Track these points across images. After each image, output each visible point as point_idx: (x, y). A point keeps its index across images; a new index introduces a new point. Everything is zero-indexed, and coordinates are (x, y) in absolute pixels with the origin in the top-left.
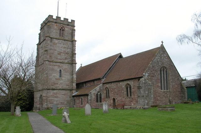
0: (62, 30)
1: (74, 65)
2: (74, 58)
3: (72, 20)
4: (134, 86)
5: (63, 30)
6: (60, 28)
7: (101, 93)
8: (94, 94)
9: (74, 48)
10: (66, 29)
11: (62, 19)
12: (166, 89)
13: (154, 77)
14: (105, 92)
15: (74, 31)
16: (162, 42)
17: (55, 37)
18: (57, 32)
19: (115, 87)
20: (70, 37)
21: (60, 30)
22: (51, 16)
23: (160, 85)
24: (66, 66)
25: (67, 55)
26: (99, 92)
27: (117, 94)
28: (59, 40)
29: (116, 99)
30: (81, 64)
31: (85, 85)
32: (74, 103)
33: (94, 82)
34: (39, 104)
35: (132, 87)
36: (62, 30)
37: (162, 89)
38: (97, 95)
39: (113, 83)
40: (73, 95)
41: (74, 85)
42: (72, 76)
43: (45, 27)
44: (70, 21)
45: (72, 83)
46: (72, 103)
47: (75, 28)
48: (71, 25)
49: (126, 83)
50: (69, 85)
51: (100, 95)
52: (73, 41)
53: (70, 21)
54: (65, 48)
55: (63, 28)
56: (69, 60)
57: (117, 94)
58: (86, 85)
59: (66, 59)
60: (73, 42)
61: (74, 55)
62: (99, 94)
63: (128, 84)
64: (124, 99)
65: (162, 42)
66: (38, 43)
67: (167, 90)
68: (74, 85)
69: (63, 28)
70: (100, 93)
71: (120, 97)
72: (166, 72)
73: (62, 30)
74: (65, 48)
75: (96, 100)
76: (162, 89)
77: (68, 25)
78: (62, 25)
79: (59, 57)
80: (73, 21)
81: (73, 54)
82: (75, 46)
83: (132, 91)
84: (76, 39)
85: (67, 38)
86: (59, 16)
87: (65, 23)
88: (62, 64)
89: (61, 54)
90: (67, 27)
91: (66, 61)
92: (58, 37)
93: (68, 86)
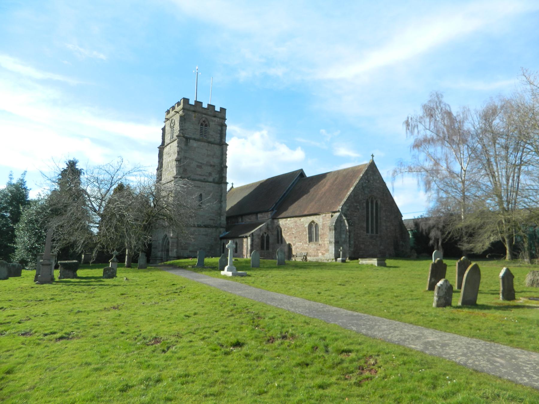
0: (204, 125)
1: (223, 185)
2: (223, 175)
3: (196, 102)
4: (323, 225)
5: (206, 126)
6: (201, 121)
7: (269, 235)
8: (258, 235)
9: (224, 156)
10: (211, 123)
11: (205, 106)
12: (375, 232)
13: (356, 212)
14: (275, 233)
15: (224, 128)
16: (373, 156)
17: (193, 137)
18: (195, 129)
19: (292, 225)
20: (217, 137)
21: (202, 125)
22: (201, 103)
23: (365, 225)
24: (209, 187)
25: (210, 169)
26: (265, 233)
27: (295, 237)
28: (199, 143)
29: (294, 245)
30: (232, 184)
31: (240, 220)
32: (222, 251)
33: (257, 215)
34: (162, 251)
35: (320, 227)
36: (204, 126)
37: (368, 232)
38: (263, 237)
39: (289, 219)
40: (221, 236)
41: (223, 219)
42: (220, 205)
43: (174, 118)
44: (217, 109)
45: (220, 216)
46: (218, 249)
47: (227, 122)
48: (220, 115)
49: (310, 219)
50: (214, 220)
51: (268, 237)
52: (223, 145)
53: (217, 109)
54: (208, 156)
55: (207, 123)
56: (215, 176)
57: (295, 237)
58: (242, 220)
59: (210, 174)
60: (223, 145)
61: (224, 169)
62: (265, 236)
63: (313, 222)
64: (307, 245)
65: (373, 156)
66: (161, 146)
67: (377, 233)
68: (222, 219)
69: (207, 123)
70: (268, 235)
71: (300, 242)
72: (377, 204)
73: (204, 125)
74: (208, 156)
75: (260, 246)
76: (368, 232)
77: (215, 116)
78: (204, 116)
79: (199, 171)
80: (223, 110)
81: (222, 169)
82: (226, 154)
83: (365, 211)
84: (227, 142)
85: (212, 140)
86: (197, 100)
87: (210, 113)
88: (203, 183)
89: (203, 166)
90: (212, 121)
91: (211, 179)
92: (197, 136)
93: (212, 221)
